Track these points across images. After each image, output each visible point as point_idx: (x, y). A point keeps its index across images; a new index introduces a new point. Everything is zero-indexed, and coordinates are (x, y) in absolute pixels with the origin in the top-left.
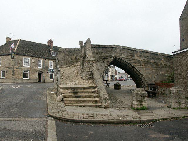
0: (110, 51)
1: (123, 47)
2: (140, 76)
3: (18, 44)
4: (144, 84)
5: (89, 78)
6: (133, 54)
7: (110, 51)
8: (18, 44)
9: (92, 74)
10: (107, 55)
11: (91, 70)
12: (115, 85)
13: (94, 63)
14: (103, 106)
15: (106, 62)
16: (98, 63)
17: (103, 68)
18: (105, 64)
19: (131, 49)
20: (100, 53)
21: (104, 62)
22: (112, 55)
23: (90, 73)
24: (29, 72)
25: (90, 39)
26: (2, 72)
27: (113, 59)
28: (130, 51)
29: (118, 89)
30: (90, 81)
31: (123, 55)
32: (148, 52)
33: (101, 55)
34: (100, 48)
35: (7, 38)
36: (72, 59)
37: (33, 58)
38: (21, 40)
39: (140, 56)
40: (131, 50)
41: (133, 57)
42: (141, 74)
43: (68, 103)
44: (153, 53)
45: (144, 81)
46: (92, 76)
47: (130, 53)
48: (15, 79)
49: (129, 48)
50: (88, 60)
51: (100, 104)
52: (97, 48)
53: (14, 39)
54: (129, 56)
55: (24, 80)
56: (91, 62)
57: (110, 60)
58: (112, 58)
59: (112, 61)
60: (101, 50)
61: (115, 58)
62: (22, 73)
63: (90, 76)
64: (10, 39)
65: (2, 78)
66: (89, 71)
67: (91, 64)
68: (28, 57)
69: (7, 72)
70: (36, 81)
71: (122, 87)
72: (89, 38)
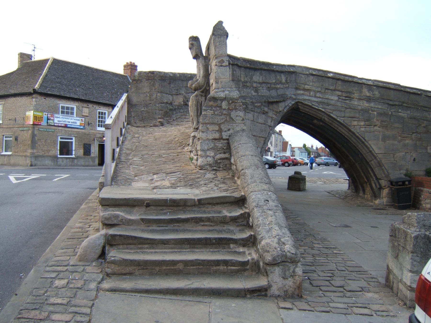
0: (284, 81)
1: (320, 73)
2: (368, 157)
3: (45, 71)
4: (377, 179)
5: (216, 162)
6: (347, 92)
7: (284, 81)
8: (45, 71)
9: (228, 149)
10: (274, 93)
11: (225, 135)
12: (291, 178)
13: (236, 109)
14: (274, 290)
15: (271, 114)
16: (250, 116)
17: (262, 131)
18: (269, 121)
19: (342, 77)
20: (255, 85)
21: (265, 113)
22: (290, 92)
23: (220, 145)
24: (74, 140)
25: (224, 25)
26: (5, 139)
27: (290, 105)
28: (339, 82)
29: (300, 189)
30: (220, 175)
31: (318, 95)
32: (392, 87)
33: (256, 91)
34: (255, 69)
35: (24, 57)
36: (171, 104)
37: (85, 105)
38: (56, 62)
39: (369, 99)
40: (344, 81)
41: (348, 102)
42: (371, 151)
43: (124, 272)
44: (409, 90)
45: (376, 170)
46: (227, 155)
47: (339, 91)
48: (37, 157)
49: (338, 77)
50: (214, 99)
51: (262, 282)
52: (246, 68)
53: (38, 57)
54: (336, 98)
55: (60, 160)
56: (224, 105)
57: (283, 107)
58: (290, 103)
59: (288, 111)
60: (257, 77)
61: (297, 103)
62: (55, 142)
63: (223, 156)
64: (30, 57)
65: (4, 153)
66: (217, 136)
67: (225, 112)
68: (72, 103)
69: (16, 139)
70: (91, 163)
71: (308, 185)
72: (220, 23)
